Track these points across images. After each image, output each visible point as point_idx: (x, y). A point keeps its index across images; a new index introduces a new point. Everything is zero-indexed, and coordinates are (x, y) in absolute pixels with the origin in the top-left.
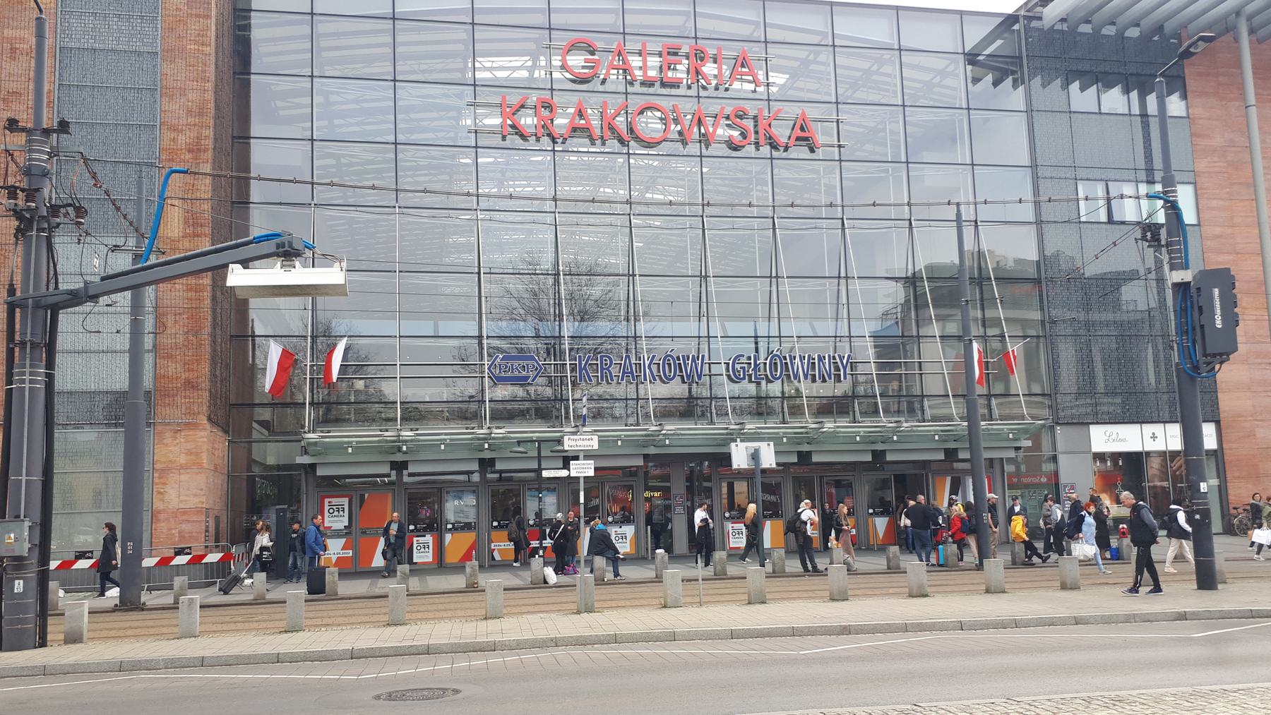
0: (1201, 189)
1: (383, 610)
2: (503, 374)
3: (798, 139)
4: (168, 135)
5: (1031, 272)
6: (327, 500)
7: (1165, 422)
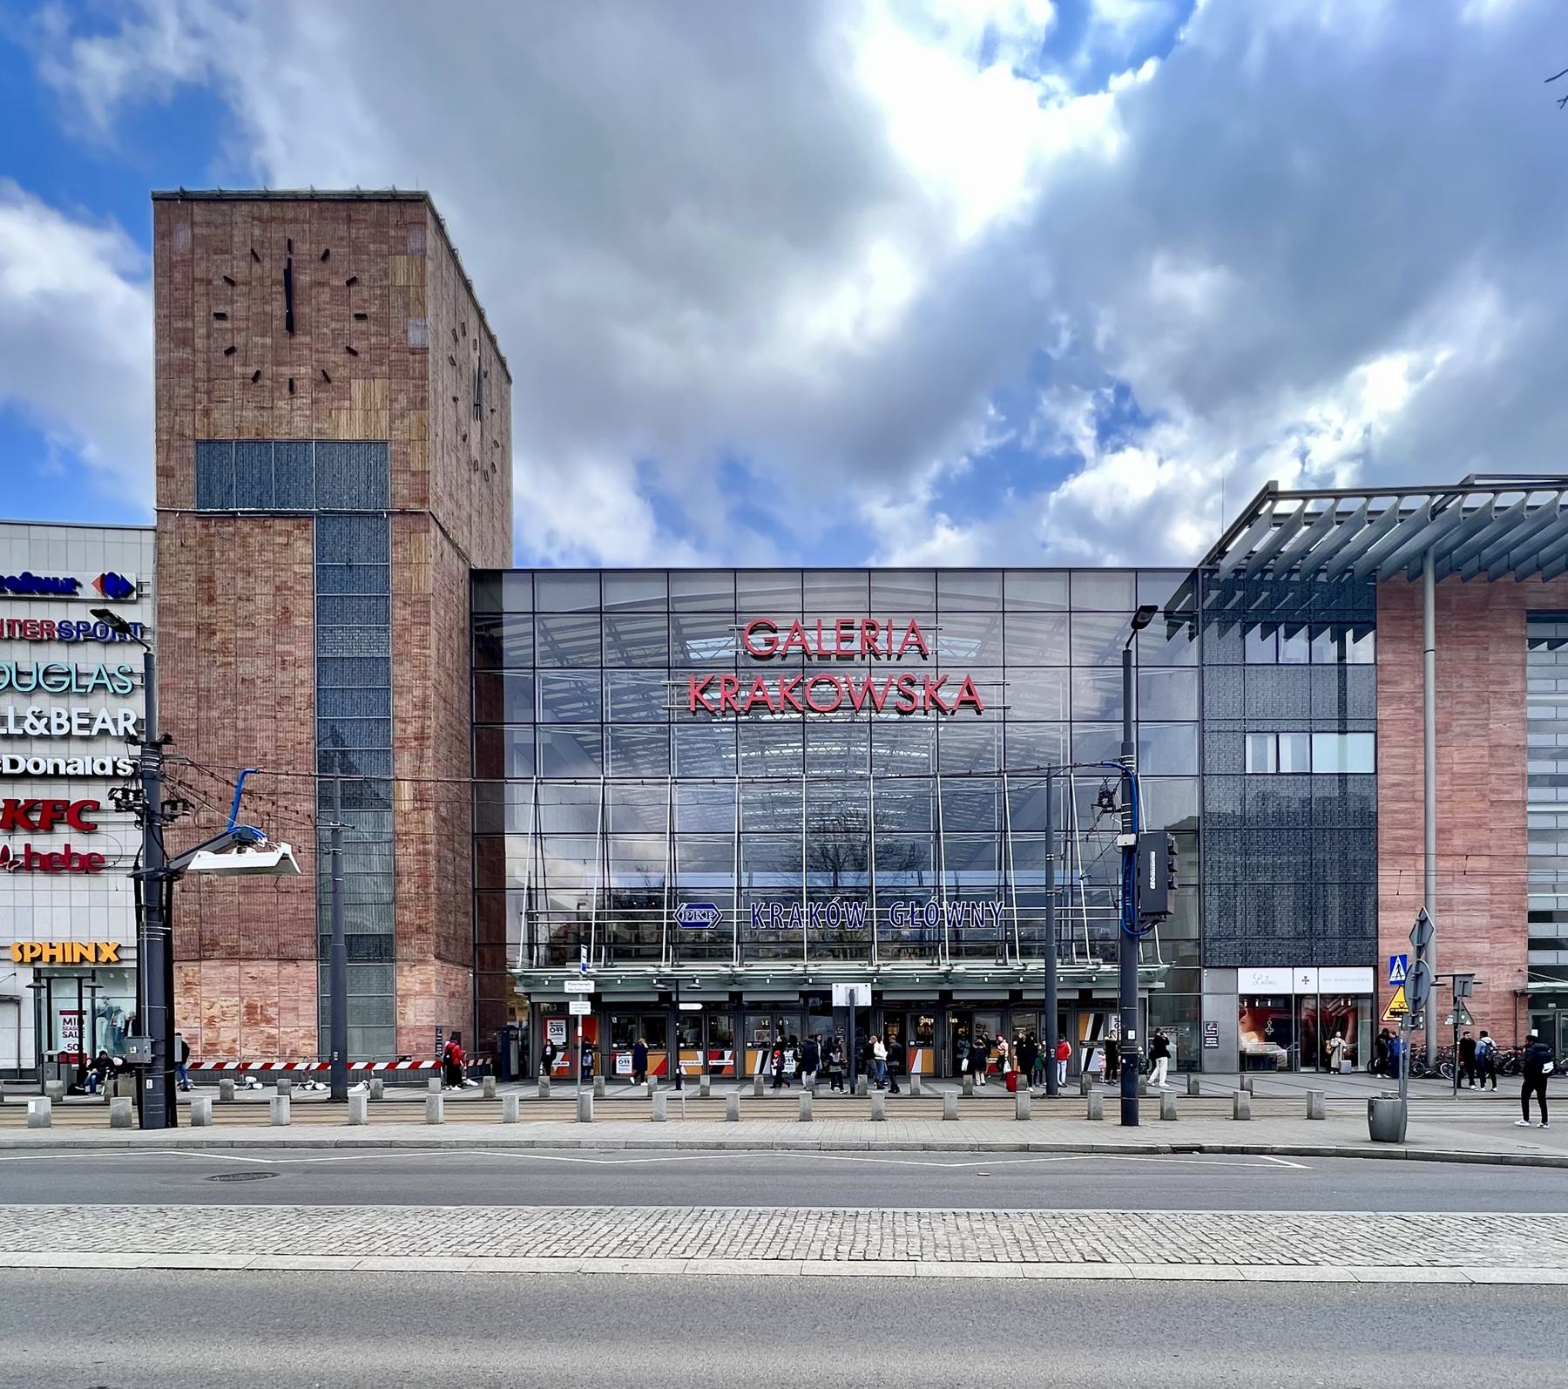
0: (1383, 737)
1: (796, 1109)
2: (687, 921)
3: (963, 702)
4: (399, 726)
5: (1194, 826)
6: (549, 1022)
7: (1318, 967)
